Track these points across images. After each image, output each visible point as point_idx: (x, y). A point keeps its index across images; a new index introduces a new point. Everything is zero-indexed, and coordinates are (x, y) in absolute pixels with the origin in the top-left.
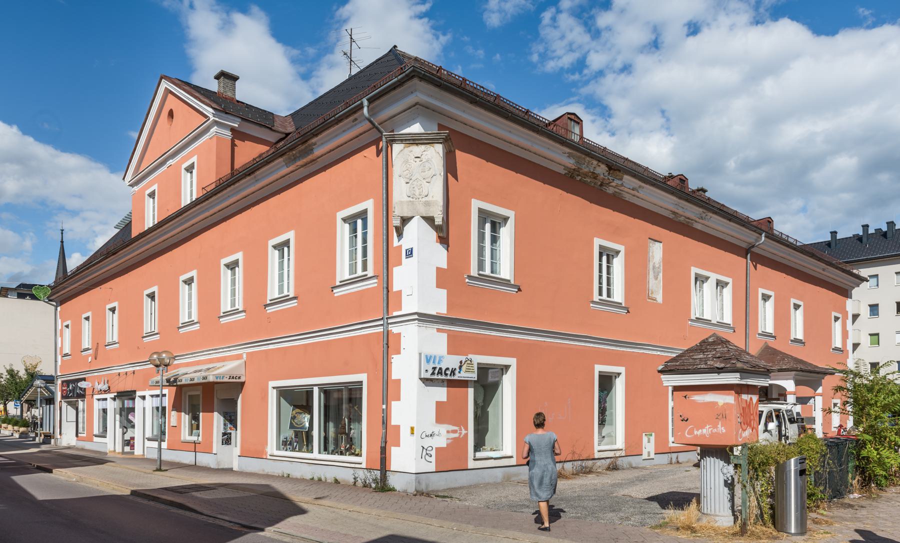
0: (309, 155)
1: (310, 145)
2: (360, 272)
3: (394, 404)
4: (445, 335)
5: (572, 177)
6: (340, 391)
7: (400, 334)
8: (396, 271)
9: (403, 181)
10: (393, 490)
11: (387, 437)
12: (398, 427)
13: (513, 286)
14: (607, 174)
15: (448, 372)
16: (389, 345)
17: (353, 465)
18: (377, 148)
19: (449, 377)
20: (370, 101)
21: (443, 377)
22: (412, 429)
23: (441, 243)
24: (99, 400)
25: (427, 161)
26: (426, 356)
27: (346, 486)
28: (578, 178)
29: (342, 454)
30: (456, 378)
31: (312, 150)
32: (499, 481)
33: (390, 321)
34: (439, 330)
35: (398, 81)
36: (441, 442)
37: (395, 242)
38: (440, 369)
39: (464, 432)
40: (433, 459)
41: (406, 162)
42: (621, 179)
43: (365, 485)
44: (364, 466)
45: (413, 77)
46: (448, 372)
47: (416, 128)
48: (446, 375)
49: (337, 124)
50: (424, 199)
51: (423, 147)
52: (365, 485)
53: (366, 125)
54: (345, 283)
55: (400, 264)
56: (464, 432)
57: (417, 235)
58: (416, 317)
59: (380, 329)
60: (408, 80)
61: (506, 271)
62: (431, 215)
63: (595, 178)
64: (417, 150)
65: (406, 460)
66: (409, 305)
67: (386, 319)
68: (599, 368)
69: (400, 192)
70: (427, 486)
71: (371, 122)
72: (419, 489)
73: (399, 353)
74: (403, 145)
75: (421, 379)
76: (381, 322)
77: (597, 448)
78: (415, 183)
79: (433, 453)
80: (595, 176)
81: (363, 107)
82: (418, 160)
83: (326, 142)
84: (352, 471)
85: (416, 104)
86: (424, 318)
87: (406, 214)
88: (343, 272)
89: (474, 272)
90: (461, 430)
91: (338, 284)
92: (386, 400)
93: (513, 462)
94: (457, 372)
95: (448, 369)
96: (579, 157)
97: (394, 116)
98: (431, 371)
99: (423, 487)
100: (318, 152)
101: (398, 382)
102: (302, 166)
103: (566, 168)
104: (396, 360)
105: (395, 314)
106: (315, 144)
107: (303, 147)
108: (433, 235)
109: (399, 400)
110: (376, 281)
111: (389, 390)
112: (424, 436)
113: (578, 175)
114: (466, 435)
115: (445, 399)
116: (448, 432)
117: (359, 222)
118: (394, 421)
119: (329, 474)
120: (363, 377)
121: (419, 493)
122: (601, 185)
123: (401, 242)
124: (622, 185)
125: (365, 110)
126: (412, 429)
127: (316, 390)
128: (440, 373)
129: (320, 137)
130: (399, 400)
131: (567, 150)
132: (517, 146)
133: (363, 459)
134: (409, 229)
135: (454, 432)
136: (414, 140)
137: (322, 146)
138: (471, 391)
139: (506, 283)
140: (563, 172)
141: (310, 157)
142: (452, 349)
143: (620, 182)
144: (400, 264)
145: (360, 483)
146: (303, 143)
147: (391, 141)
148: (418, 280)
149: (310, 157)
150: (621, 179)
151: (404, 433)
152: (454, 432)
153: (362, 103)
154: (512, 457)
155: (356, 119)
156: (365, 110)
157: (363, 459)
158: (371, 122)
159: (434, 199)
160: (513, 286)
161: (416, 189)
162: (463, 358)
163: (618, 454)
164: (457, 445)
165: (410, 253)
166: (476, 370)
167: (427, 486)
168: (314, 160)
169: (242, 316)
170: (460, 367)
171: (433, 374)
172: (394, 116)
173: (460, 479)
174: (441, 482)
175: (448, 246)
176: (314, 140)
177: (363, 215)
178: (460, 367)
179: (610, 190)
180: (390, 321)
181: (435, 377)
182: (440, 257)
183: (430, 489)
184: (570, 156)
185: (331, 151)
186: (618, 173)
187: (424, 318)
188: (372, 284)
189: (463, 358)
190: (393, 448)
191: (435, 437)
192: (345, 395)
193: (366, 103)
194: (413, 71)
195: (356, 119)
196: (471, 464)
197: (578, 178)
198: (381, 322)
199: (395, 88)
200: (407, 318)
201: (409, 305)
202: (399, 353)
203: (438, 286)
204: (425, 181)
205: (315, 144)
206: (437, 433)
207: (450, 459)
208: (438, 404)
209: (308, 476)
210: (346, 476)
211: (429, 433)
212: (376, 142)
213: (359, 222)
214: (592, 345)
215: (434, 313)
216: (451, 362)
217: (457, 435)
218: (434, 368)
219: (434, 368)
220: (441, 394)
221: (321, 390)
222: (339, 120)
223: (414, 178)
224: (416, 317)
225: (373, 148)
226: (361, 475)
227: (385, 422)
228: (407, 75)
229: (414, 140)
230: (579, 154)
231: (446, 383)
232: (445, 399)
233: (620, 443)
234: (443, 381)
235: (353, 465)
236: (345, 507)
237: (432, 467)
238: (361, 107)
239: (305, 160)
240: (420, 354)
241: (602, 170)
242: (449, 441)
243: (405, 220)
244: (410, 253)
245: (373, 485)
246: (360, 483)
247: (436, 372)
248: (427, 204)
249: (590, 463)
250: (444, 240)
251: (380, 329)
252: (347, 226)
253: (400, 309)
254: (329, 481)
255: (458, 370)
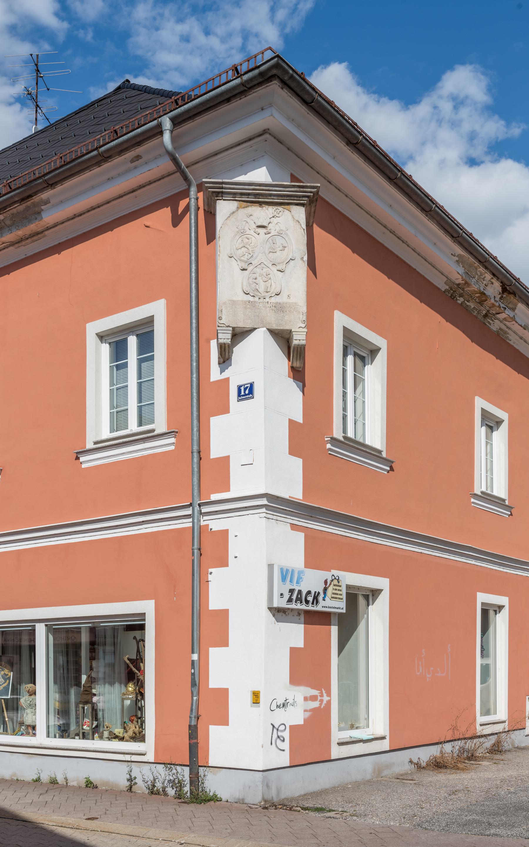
0: (30, 222)
1: (35, 205)
2: (133, 426)
3: (215, 654)
4: (301, 536)
5: (453, 297)
6: (20, 633)
7: (226, 532)
8: (217, 424)
9: (236, 266)
10: (215, 799)
11: (203, 708)
12: (224, 693)
13: (385, 461)
14: (498, 299)
15: (310, 599)
16: (208, 550)
17: (128, 758)
18: (174, 211)
19: (310, 608)
20: (176, 122)
21: (304, 607)
22: (256, 695)
23: (294, 378)
24: (342, 609)
25: (279, 234)
26: (282, 570)
27: (112, 792)
28: (460, 300)
29: (84, 736)
30: (319, 608)
31: (39, 213)
32: (368, 777)
33: (204, 510)
34: (294, 527)
35: (242, 84)
36: (296, 716)
37: (215, 374)
38: (300, 592)
39: (326, 698)
40: (286, 745)
41: (242, 233)
42: (513, 309)
43: (153, 791)
44: (150, 757)
45: (269, 79)
46: (310, 599)
47: (260, 175)
48: (307, 602)
49: (98, 164)
50: (273, 300)
51: (270, 210)
52: (153, 791)
53: (166, 165)
54: (102, 446)
55: (225, 410)
56: (326, 698)
57: (257, 360)
58: (264, 502)
59: (187, 524)
60: (260, 84)
61: (375, 436)
62: (287, 327)
63: (481, 303)
64: (262, 214)
65: (244, 747)
66: (241, 484)
67: (198, 505)
68: (482, 598)
69: (230, 285)
70: (279, 791)
71: (175, 160)
72: (268, 797)
73: (223, 563)
74: (235, 204)
75: (270, 609)
76: (189, 512)
77: (480, 719)
78: (258, 270)
79: (286, 735)
80: (483, 297)
81: (161, 133)
82: (262, 231)
83: (68, 199)
84: (124, 768)
85: (265, 131)
86: (277, 505)
87: (242, 323)
88: (99, 425)
89: (338, 434)
90: (322, 696)
91: (90, 445)
92: (197, 643)
93: (385, 745)
94: (320, 598)
95: (309, 593)
96: (471, 265)
97: (216, 154)
98: (287, 596)
99: (273, 795)
100: (49, 217)
101: (224, 614)
102: (12, 244)
103: (449, 281)
104: (217, 577)
105: (214, 497)
106: (47, 202)
107: (21, 208)
108: (282, 364)
109: (225, 644)
110: (173, 440)
111: (206, 628)
112: (274, 707)
113: (461, 296)
114: (329, 703)
115: (301, 644)
116: (306, 699)
117: (132, 342)
118: (215, 681)
119: (75, 772)
120: (147, 607)
121: (269, 805)
122: (486, 316)
123: (226, 374)
124: (513, 319)
125: (167, 137)
126: (256, 695)
127: (41, 630)
128: (299, 599)
129: (59, 188)
130: (225, 644)
131: (459, 250)
132: (392, 232)
133: (148, 748)
134: (240, 351)
135: (313, 698)
136: (256, 195)
137: (59, 207)
138: (334, 630)
139: (373, 453)
140: (443, 287)
141: (33, 227)
142: (312, 561)
143: (511, 314)
144: (225, 410)
145: (141, 787)
146: (23, 200)
147: (216, 194)
148: (254, 441)
149: (33, 227)
150: (513, 309)
151: (238, 705)
152: (313, 698)
153: (160, 125)
154: (383, 738)
155: (138, 157)
156: (167, 137)
157: (148, 748)
158: (175, 160)
159: (292, 300)
160: (385, 461)
161: (260, 280)
162: (328, 575)
163: (499, 728)
164: (319, 719)
165: (247, 392)
166: (344, 596)
167: (279, 791)
168: (38, 233)
169: (167, 445)
170: (325, 590)
171: (290, 600)
172: (216, 154)
173: (320, 777)
174: (298, 784)
175: (304, 386)
176: (44, 196)
177: (144, 331)
178: (325, 590)
179: (495, 326)
180: (204, 510)
181: (293, 606)
182: (291, 402)
183: (283, 796)
184: (460, 261)
185: (75, 217)
186: (512, 297)
187: (277, 505)
188: (167, 445)
189: (328, 575)
190: (212, 728)
191: (289, 708)
192: (85, 638)
193: (167, 123)
194: (277, 66)
195: (138, 157)
196: (336, 752)
197: (460, 300)
198: (189, 512)
199: (228, 100)
200: (245, 504)
201: (241, 484)
202: (223, 563)
203: (292, 452)
204: (274, 269)
205: (47, 202)
206: (291, 701)
207: (309, 743)
208: (293, 650)
209: (29, 776)
210: (116, 775)
211: (281, 702)
212: (171, 201)
213: (132, 342)
214: (473, 562)
215: (286, 496)
216: (312, 581)
217: (316, 704)
218: (292, 591)
219: (292, 591)
220: (295, 634)
221: (50, 629)
222: (105, 158)
223: (255, 262)
224: (264, 502)
225: (166, 213)
226: (143, 775)
227: (197, 679)
228: (261, 74)
229: (256, 196)
230: (472, 259)
231: (302, 616)
232: (301, 644)
233: (502, 712)
234: (299, 612)
235: (128, 758)
236: (165, 835)
237: (284, 760)
238: (158, 131)
239: (20, 233)
240: (271, 567)
241: (494, 289)
242: (308, 714)
243: (239, 335)
244: (247, 392)
245: (171, 792)
246: (141, 787)
247: (294, 597)
248: (280, 308)
249: (469, 744)
250: (298, 374)
251: (187, 524)
252: (105, 349)
253: (227, 489)
254: (73, 783)
255: (322, 595)
